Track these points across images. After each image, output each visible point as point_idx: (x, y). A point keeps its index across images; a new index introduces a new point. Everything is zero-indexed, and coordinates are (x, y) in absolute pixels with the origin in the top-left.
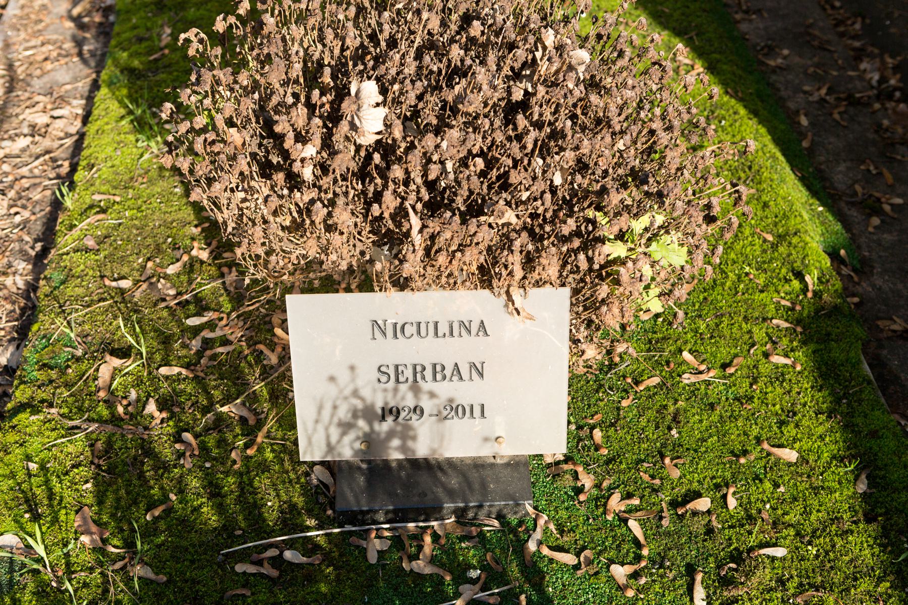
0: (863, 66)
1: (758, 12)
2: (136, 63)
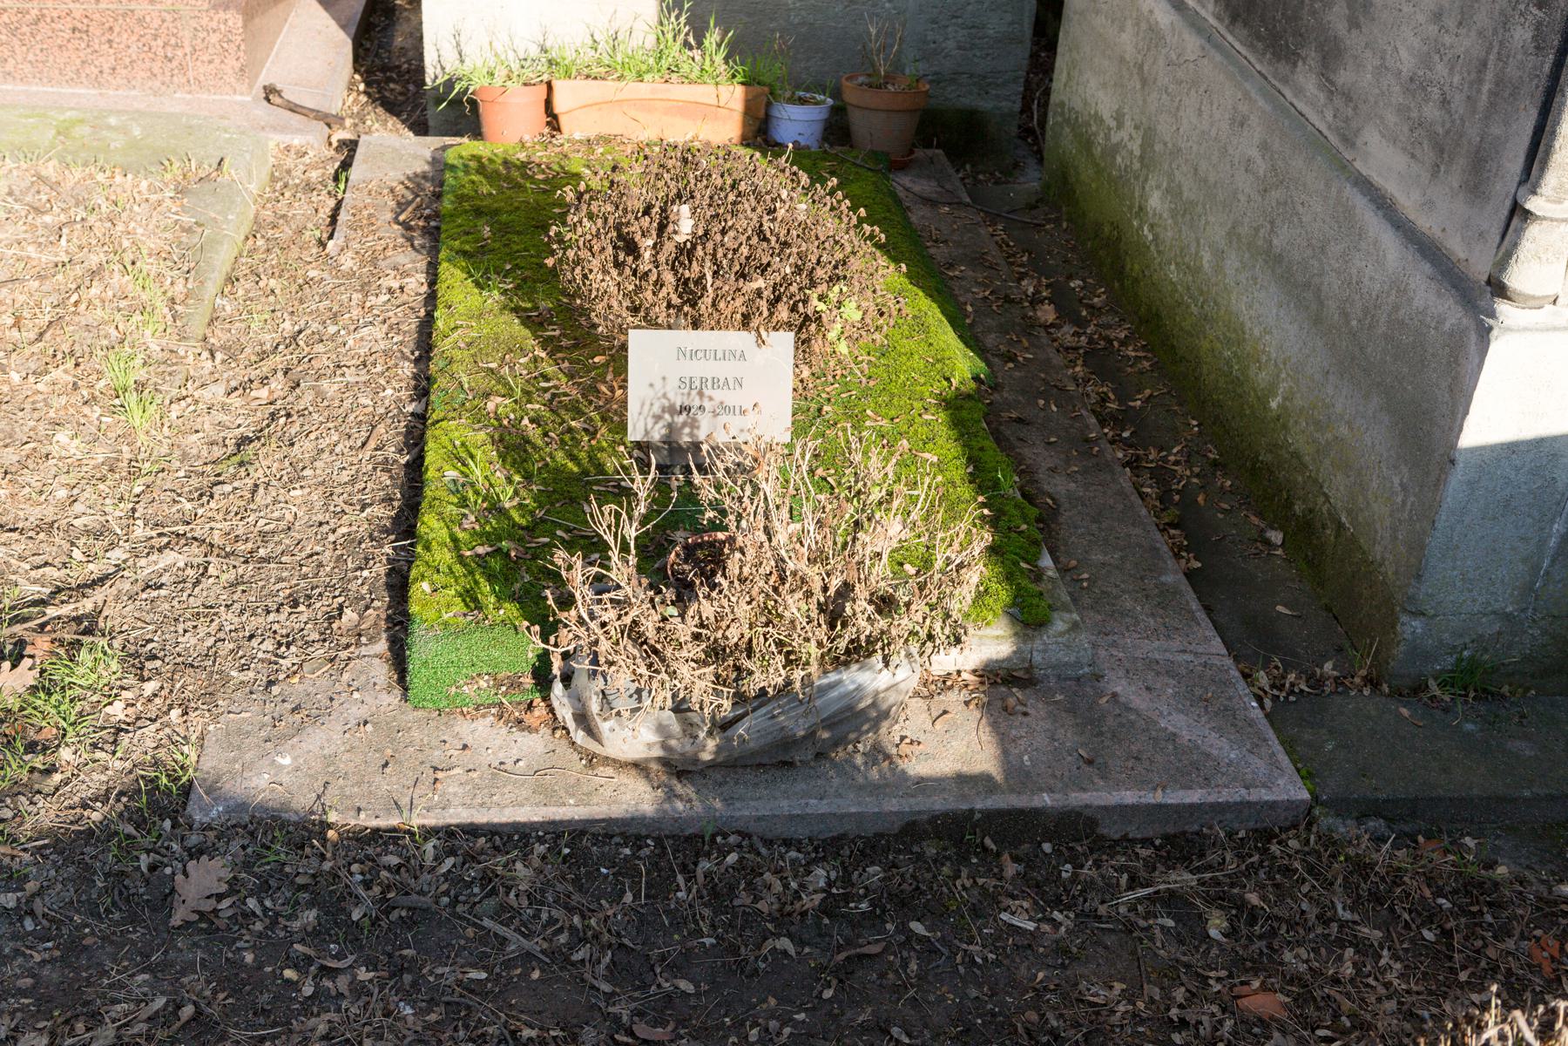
0: (1024, 283)
1: (945, 242)
2: (467, 247)
